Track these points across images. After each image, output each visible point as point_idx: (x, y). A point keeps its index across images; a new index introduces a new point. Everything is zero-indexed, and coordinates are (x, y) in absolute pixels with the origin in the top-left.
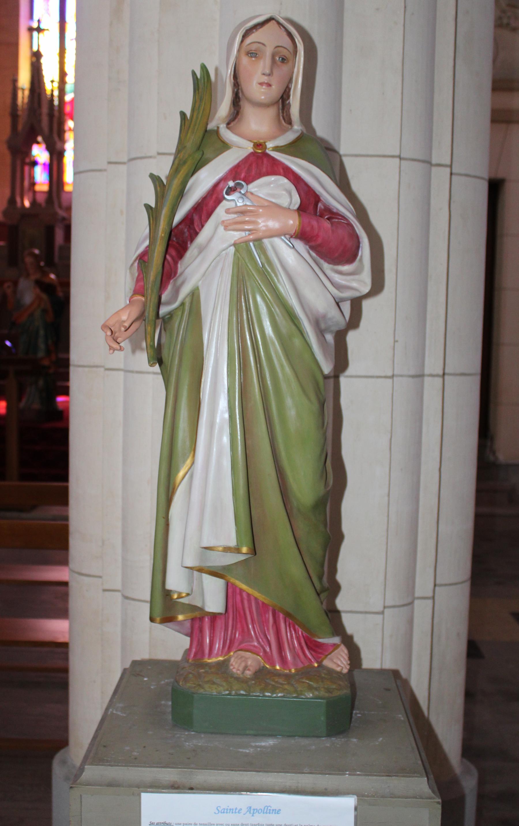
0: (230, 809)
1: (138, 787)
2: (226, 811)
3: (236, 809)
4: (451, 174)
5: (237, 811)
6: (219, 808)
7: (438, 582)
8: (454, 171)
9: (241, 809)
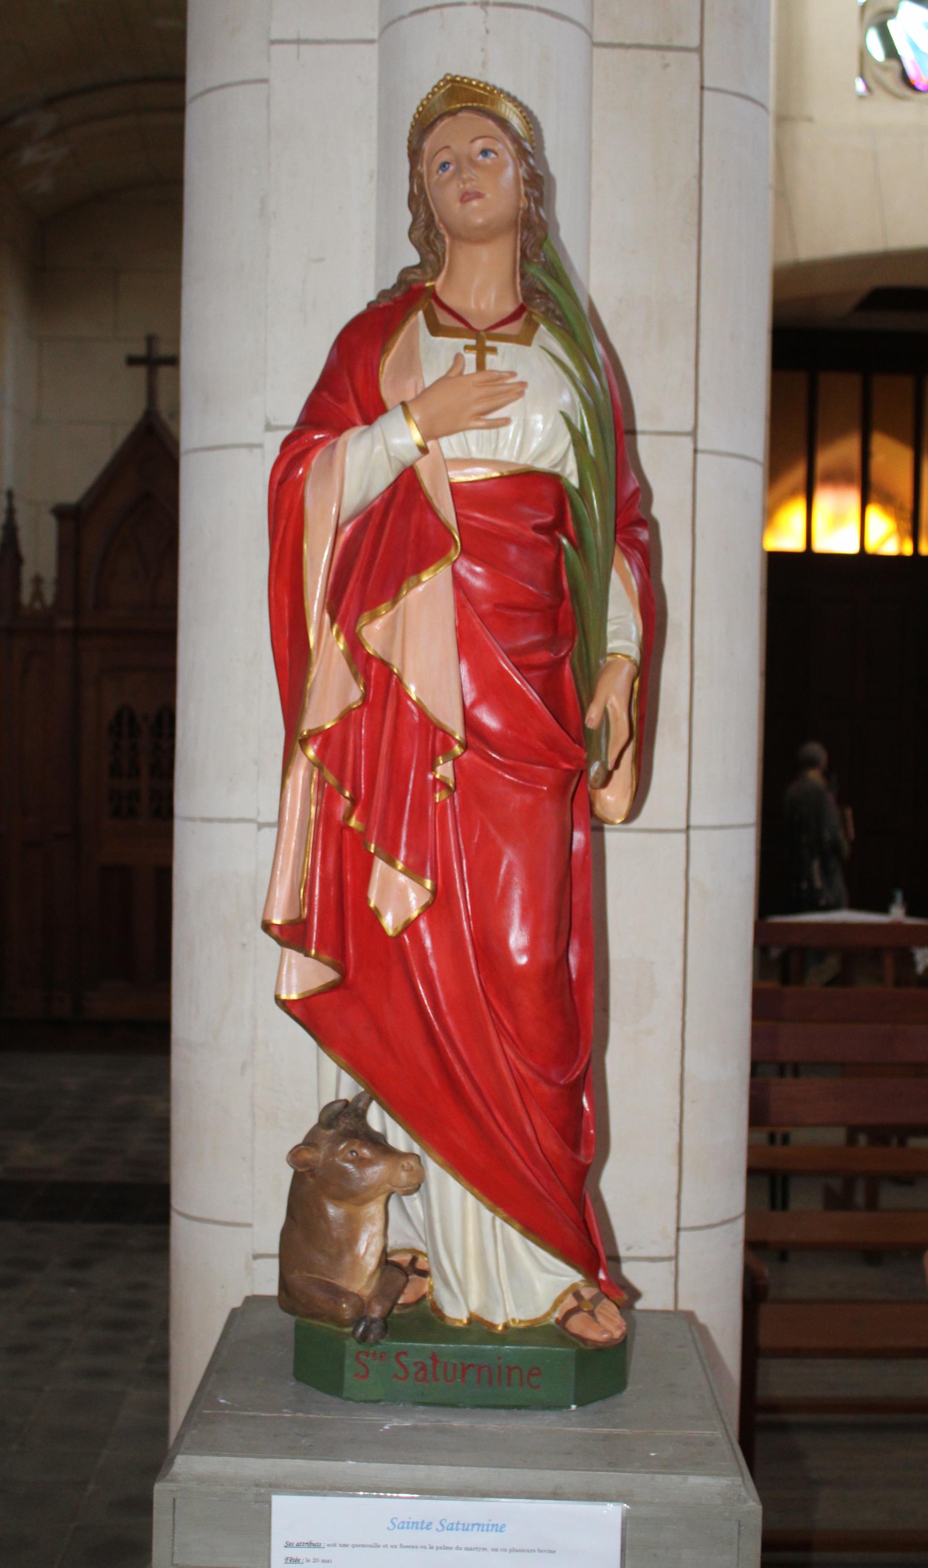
0: (413, 1523)
1: (271, 1486)
2: (406, 1525)
3: (423, 1522)
4: (696, 451)
5: (425, 1525)
6: (394, 1521)
7: (683, 1224)
8: (700, 446)
9: (431, 1523)
